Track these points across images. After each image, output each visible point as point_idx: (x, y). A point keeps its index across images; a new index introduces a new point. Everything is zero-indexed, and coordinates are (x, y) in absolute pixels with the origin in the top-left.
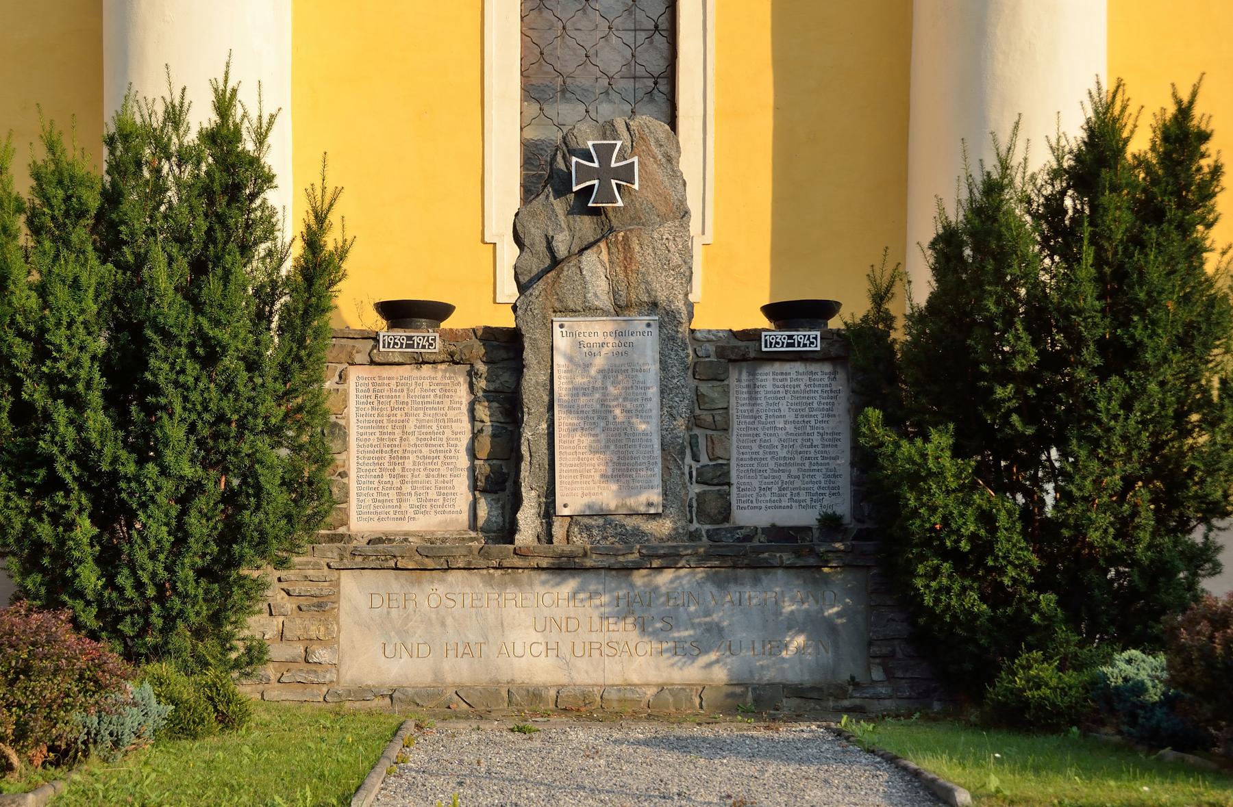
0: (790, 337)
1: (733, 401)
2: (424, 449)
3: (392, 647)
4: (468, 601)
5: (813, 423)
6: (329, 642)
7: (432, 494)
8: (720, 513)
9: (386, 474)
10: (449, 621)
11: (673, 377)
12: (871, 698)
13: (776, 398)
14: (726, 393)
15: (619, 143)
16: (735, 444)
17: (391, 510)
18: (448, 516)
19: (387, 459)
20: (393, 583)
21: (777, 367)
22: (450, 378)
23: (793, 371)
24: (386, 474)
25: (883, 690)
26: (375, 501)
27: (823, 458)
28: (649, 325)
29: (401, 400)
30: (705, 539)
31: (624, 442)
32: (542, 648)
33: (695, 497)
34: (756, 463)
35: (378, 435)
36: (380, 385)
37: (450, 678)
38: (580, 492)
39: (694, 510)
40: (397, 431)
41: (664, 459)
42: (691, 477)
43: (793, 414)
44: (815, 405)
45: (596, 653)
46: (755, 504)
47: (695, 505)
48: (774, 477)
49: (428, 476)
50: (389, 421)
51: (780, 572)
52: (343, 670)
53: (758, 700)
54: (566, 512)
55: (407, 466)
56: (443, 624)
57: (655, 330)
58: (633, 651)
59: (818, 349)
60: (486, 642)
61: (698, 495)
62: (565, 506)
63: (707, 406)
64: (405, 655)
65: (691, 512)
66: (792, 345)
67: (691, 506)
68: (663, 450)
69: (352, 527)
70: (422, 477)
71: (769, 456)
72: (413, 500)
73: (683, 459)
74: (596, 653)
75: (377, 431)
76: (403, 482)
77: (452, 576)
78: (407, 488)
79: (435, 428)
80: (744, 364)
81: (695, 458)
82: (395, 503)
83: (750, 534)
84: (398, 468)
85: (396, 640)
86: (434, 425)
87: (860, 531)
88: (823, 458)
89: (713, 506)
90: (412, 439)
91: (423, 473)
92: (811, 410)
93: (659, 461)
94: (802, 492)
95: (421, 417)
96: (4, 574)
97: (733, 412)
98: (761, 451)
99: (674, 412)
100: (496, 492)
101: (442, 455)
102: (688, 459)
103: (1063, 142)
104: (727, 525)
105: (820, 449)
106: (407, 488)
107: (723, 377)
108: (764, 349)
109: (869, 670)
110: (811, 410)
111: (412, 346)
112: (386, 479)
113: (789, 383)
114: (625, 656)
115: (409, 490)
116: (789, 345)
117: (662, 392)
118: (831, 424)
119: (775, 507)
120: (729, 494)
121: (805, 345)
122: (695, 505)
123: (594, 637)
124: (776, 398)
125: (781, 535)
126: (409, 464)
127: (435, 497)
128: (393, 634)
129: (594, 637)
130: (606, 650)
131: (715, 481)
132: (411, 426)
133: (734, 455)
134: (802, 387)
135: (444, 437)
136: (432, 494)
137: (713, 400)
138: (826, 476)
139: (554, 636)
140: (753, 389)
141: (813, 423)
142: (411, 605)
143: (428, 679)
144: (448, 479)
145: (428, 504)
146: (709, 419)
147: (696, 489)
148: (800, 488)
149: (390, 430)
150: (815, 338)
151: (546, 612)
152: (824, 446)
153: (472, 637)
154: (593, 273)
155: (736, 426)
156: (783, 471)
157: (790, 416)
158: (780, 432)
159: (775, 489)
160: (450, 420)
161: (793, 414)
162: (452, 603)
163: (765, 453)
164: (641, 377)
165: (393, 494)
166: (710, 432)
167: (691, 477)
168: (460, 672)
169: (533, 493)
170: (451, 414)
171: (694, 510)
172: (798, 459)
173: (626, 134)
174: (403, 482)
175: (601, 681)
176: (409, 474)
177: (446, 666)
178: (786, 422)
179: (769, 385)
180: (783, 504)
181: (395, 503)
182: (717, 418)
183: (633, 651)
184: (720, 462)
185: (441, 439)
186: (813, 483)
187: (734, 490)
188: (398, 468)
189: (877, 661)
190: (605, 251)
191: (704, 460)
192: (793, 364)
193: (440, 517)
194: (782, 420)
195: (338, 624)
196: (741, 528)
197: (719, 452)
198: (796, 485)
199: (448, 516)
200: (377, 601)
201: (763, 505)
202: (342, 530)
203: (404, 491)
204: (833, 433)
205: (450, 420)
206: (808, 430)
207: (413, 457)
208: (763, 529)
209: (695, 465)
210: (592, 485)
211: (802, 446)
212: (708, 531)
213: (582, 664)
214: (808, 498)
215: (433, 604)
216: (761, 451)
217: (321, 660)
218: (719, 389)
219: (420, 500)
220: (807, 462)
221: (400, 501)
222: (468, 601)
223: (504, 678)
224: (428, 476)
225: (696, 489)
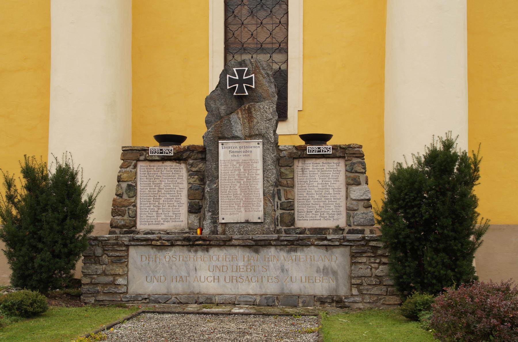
0: (319, 148)
1: (296, 175)
2: (167, 195)
3: (150, 278)
4: (181, 259)
5: (329, 184)
6: (125, 275)
7: (171, 214)
8: (290, 222)
9: (152, 206)
10: (174, 267)
11: (269, 165)
12: (352, 302)
13: (314, 174)
14: (293, 172)
15: (246, 69)
16: (296, 193)
17: (154, 220)
18: (177, 223)
19: (152, 199)
20: (152, 252)
21: (314, 161)
22: (178, 166)
23: (321, 162)
24: (152, 206)
25: (358, 299)
26: (147, 216)
27: (334, 199)
28: (258, 144)
29: (158, 175)
30: (283, 233)
31: (248, 192)
32: (212, 278)
33: (279, 215)
34: (305, 201)
35: (149, 189)
36: (150, 169)
37: (174, 291)
38: (229, 213)
39: (279, 220)
40: (156, 188)
41: (264, 199)
42: (278, 207)
43: (321, 180)
44: (331, 177)
45: (234, 281)
46: (305, 218)
47: (279, 218)
48: (313, 207)
49: (169, 206)
50: (153, 184)
51: (312, 247)
52: (129, 288)
53: (5, 251)
54: (223, 221)
55: (160, 202)
56: (171, 268)
57: (261, 146)
58: (250, 280)
59: (331, 153)
60: (189, 276)
61: (281, 214)
62: (223, 219)
63: (284, 177)
64: (155, 281)
65: (277, 221)
66: (320, 151)
67: (277, 219)
68: (264, 195)
69: (138, 227)
70: (167, 207)
71: (311, 198)
72: (163, 216)
73: (274, 200)
74: (234, 281)
75: (148, 188)
76: (158, 209)
77: (174, 249)
78: (160, 211)
79: (172, 187)
80: (301, 160)
81: (280, 199)
82: (155, 217)
83: (303, 231)
84: (157, 203)
85: (152, 275)
86: (172, 185)
87: (349, 230)
88: (334, 199)
89: (287, 219)
90: (163, 191)
91: (167, 205)
92: (329, 178)
93: (262, 200)
94: (325, 213)
95: (166, 182)
96: (516, 322)
97: (296, 180)
98: (308, 196)
99: (269, 180)
100: (197, 213)
101: (175, 198)
102: (276, 199)
103: (35, 162)
104: (292, 227)
105: (333, 195)
106: (160, 211)
107: (291, 165)
108: (308, 153)
109: (351, 290)
110: (329, 178)
111: (162, 153)
112: (152, 207)
113: (319, 167)
114: (247, 282)
115: (161, 212)
116: (318, 151)
117: (264, 171)
118: (337, 185)
119: (314, 220)
120: (294, 214)
121: (325, 152)
122: (279, 218)
123: (234, 274)
124: (314, 174)
125: (319, 232)
126: (161, 201)
127: (172, 215)
128: (150, 272)
129: (234, 274)
130: (239, 280)
131: (288, 208)
132: (162, 186)
133: (296, 198)
134: (325, 169)
135: (176, 190)
136: (171, 214)
137: (287, 175)
138: (335, 206)
139: (217, 274)
140: (303, 170)
141: (329, 184)
142: (158, 260)
143: (165, 291)
144: (177, 207)
145: (169, 218)
146: (285, 183)
147: (279, 212)
148: (324, 212)
149: (154, 187)
150: (330, 149)
151: (214, 263)
152: (334, 194)
153: (184, 274)
154: (235, 122)
155: (297, 185)
156: (317, 204)
157: (320, 181)
158: (315, 188)
159: (314, 212)
160: (178, 183)
161: (321, 180)
162: (175, 259)
163: (309, 197)
164: (255, 165)
165: (154, 214)
166: (286, 188)
167: (278, 207)
168: (178, 288)
169: (210, 214)
170: (179, 181)
171: (279, 220)
172: (323, 199)
173: (250, 66)
174: (158, 209)
175: (237, 293)
176: (161, 205)
177: (172, 285)
178: (318, 184)
179: (311, 168)
180: (317, 218)
181: (155, 217)
182: (288, 182)
183: (250, 280)
184: (290, 200)
185: (175, 191)
186: (330, 209)
187: (296, 213)
188: (157, 203)
189: (355, 286)
190: (240, 113)
191: (283, 199)
192: (312, 159)
193: (174, 223)
194: (316, 183)
195: (128, 268)
196: (298, 228)
197: (289, 196)
198: (322, 210)
199: (177, 223)
200: (144, 258)
201: (309, 219)
202: (133, 229)
203: (159, 212)
204: (338, 188)
205: (178, 183)
206: (328, 187)
207: (163, 199)
208: (308, 229)
209: (279, 202)
210: (234, 210)
211: (325, 194)
212: (285, 229)
213: (229, 285)
214: (328, 216)
215: (167, 260)
216: (308, 196)
217: (120, 283)
218: (289, 170)
219: (166, 216)
220: (327, 201)
221: (157, 216)
222: (181, 259)
223: (196, 291)
224: (169, 206)
225: (279, 212)
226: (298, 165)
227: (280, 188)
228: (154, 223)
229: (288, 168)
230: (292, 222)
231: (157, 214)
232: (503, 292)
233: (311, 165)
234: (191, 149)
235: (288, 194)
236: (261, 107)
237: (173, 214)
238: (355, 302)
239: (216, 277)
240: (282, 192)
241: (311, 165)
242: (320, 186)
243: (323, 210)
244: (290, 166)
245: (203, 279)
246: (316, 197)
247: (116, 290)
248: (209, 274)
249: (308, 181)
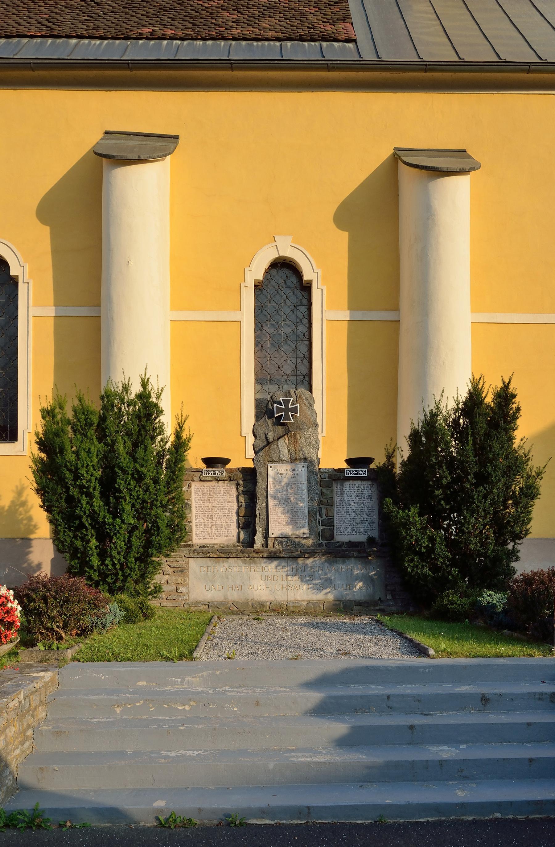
0: (356, 471)
2: (220, 513)
4: (237, 570)
6: (185, 585)
7: (223, 529)
10: (230, 577)
14: (332, 492)
26: (202, 532)
28: (303, 467)
32: (264, 587)
51: (353, 559)
52: (190, 595)
56: (227, 578)
57: (305, 468)
64: (213, 589)
66: (357, 474)
67: (319, 534)
70: (219, 523)
72: (216, 532)
76: (212, 525)
78: (214, 527)
79: (224, 505)
81: (321, 516)
86: (224, 504)
89: (327, 534)
90: (216, 509)
91: (220, 522)
92: (364, 498)
97: (335, 499)
102: (318, 517)
106: (214, 527)
110: (364, 498)
111: (215, 474)
112: (206, 524)
116: (355, 474)
117: (308, 492)
123: (284, 583)
125: (352, 545)
129: (284, 583)
130: (288, 588)
132: (215, 504)
133: (335, 515)
136: (223, 529)
137: (327, 495)
140: (342, 491)
142: (215, 571)
143: (222, 598)
151: (266, 573)
153: (238, 583)
154: (283, 447)
157: (356, 501)
160: (230, 502)
164: (300, 486)
165: (208, 529)
166: (326, 507)
168: (234, 596)
173: (294, 396)
174: (212, 525)
177: (229, 594)
187: (335, 528)
191: (324, 517)
196: (338, 542)
200: (203, 569)
202: (189, 543)
205: (230, 502)
207: (216, 516)
212: (325, 543)
213: (279, 593)
220: (362, 518)
222: (237, 570)
226: (336, 487)
227: (321, 506)
228: (208, 537)
229: (328, 488)
230: (332, 537)
231: (211, 529)
232: (40, 705)
233: (348, 486)
234: (54, 460)
235: (329, 512)
236: (306, 433)
237: (226, 529)
238: (390, 606)
239: (268, 586)
240: (323, 510)
241: (348, 486)
242: (356, 505)
243: (359, 526)
244: (329, 486)
245: (256, 588)
246: (353, 514)
247: (179, 598)
248: (262, 583)
249: (346, 500)
